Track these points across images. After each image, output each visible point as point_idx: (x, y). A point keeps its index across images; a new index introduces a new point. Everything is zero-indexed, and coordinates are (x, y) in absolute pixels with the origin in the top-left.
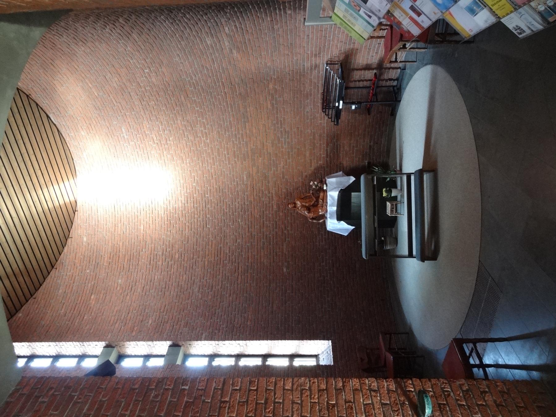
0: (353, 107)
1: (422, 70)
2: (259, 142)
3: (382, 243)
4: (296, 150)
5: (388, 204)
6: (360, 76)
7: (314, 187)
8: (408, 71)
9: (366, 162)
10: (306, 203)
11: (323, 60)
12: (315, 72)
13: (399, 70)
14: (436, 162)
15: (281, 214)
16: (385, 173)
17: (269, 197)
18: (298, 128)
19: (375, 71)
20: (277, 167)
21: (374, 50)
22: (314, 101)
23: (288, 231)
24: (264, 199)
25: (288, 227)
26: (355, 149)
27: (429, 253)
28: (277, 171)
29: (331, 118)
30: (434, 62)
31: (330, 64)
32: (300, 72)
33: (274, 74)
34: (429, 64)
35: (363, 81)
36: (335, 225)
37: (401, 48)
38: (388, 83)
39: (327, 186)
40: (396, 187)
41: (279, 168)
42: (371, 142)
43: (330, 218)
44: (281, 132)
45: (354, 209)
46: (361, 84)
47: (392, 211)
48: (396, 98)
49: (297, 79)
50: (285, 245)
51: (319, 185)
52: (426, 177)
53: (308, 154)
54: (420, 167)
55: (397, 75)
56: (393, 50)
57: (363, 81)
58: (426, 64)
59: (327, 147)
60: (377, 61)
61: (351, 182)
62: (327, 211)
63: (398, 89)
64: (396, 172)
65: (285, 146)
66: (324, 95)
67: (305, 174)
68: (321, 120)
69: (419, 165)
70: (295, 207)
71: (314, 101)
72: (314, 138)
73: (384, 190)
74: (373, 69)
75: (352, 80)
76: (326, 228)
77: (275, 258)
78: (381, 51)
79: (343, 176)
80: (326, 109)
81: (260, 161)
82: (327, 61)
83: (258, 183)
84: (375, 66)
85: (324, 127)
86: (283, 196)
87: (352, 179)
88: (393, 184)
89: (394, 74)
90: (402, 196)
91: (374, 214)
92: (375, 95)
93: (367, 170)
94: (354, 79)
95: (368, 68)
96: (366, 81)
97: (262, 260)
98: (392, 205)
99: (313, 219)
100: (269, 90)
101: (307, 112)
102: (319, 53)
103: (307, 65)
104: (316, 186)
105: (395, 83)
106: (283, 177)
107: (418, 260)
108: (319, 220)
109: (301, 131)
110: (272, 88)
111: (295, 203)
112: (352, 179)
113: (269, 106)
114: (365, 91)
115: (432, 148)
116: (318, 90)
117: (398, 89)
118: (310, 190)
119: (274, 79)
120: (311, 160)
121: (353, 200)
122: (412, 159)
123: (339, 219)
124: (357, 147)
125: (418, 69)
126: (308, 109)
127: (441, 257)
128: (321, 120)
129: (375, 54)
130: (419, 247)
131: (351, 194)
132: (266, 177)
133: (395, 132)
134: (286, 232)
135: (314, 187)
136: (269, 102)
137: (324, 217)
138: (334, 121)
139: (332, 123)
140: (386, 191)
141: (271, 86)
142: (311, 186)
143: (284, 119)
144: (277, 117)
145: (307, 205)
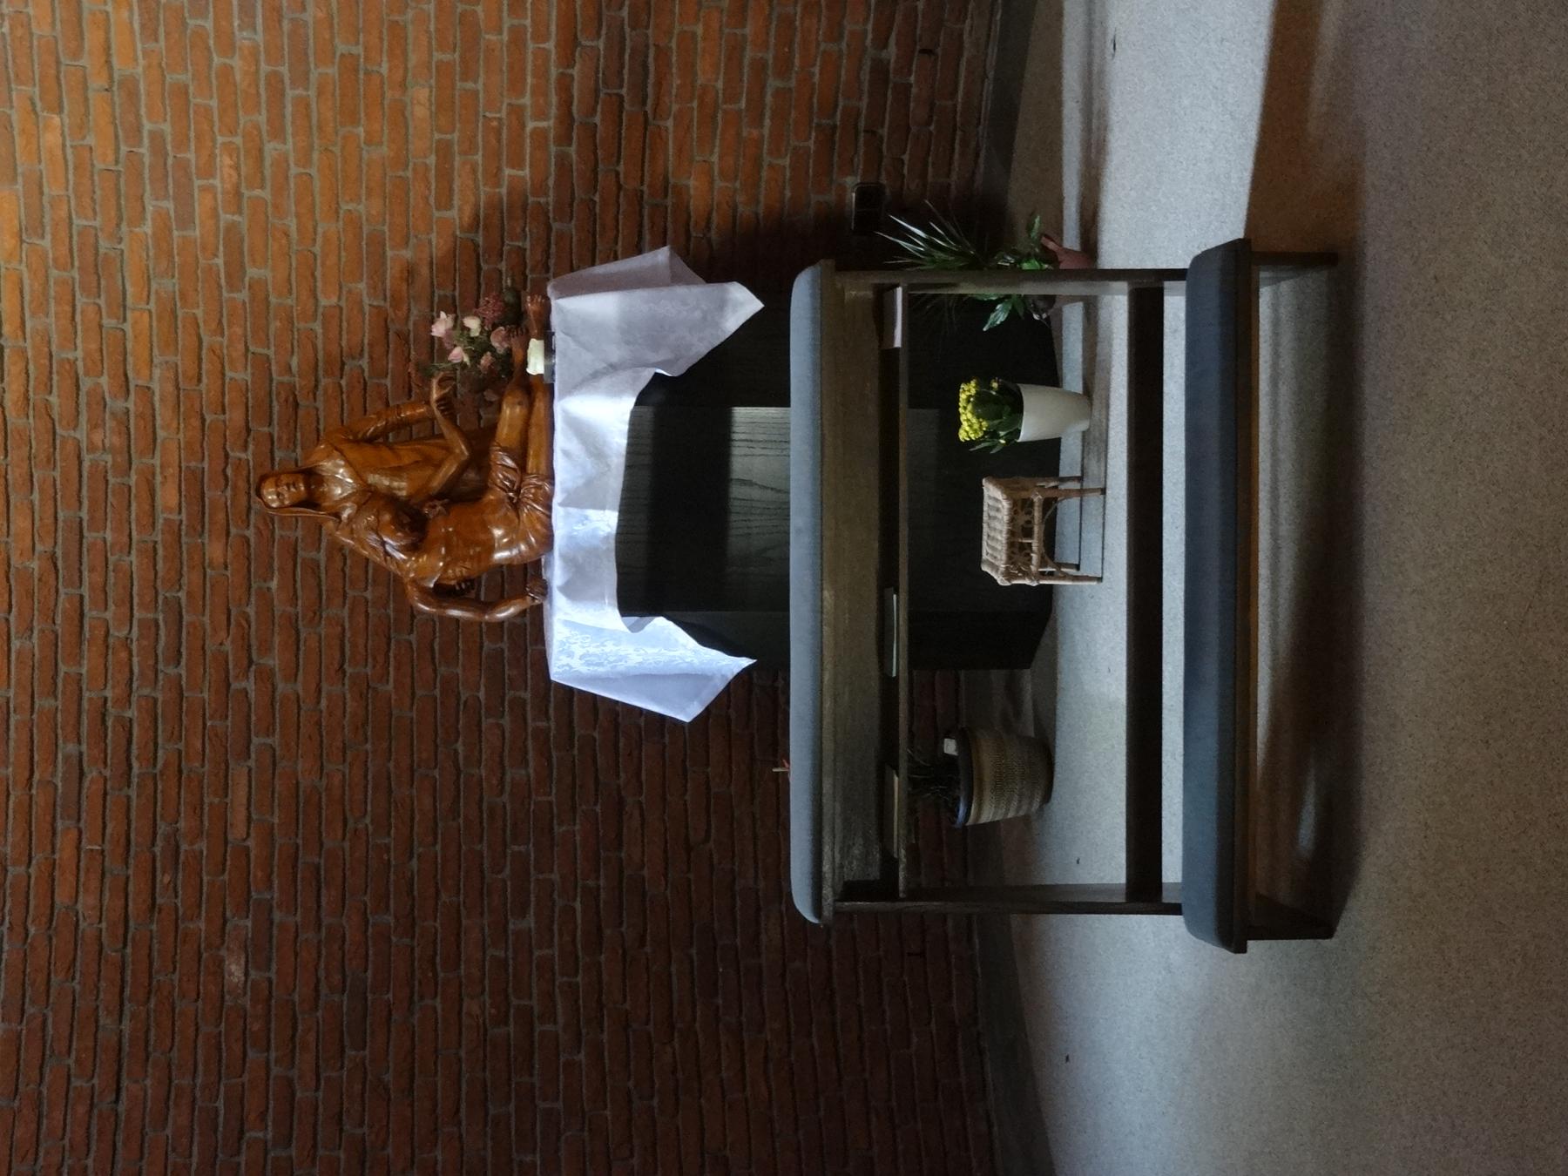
7: (458, 354)
10: (396, 472)
23: (266, 676)
25: (266, 648)
70: (311, 501)
99: (444, 593)
104: (478, 347)
111: (312, 476)
134: (251, 686)
142: (437, 349)
145: (402, 487)
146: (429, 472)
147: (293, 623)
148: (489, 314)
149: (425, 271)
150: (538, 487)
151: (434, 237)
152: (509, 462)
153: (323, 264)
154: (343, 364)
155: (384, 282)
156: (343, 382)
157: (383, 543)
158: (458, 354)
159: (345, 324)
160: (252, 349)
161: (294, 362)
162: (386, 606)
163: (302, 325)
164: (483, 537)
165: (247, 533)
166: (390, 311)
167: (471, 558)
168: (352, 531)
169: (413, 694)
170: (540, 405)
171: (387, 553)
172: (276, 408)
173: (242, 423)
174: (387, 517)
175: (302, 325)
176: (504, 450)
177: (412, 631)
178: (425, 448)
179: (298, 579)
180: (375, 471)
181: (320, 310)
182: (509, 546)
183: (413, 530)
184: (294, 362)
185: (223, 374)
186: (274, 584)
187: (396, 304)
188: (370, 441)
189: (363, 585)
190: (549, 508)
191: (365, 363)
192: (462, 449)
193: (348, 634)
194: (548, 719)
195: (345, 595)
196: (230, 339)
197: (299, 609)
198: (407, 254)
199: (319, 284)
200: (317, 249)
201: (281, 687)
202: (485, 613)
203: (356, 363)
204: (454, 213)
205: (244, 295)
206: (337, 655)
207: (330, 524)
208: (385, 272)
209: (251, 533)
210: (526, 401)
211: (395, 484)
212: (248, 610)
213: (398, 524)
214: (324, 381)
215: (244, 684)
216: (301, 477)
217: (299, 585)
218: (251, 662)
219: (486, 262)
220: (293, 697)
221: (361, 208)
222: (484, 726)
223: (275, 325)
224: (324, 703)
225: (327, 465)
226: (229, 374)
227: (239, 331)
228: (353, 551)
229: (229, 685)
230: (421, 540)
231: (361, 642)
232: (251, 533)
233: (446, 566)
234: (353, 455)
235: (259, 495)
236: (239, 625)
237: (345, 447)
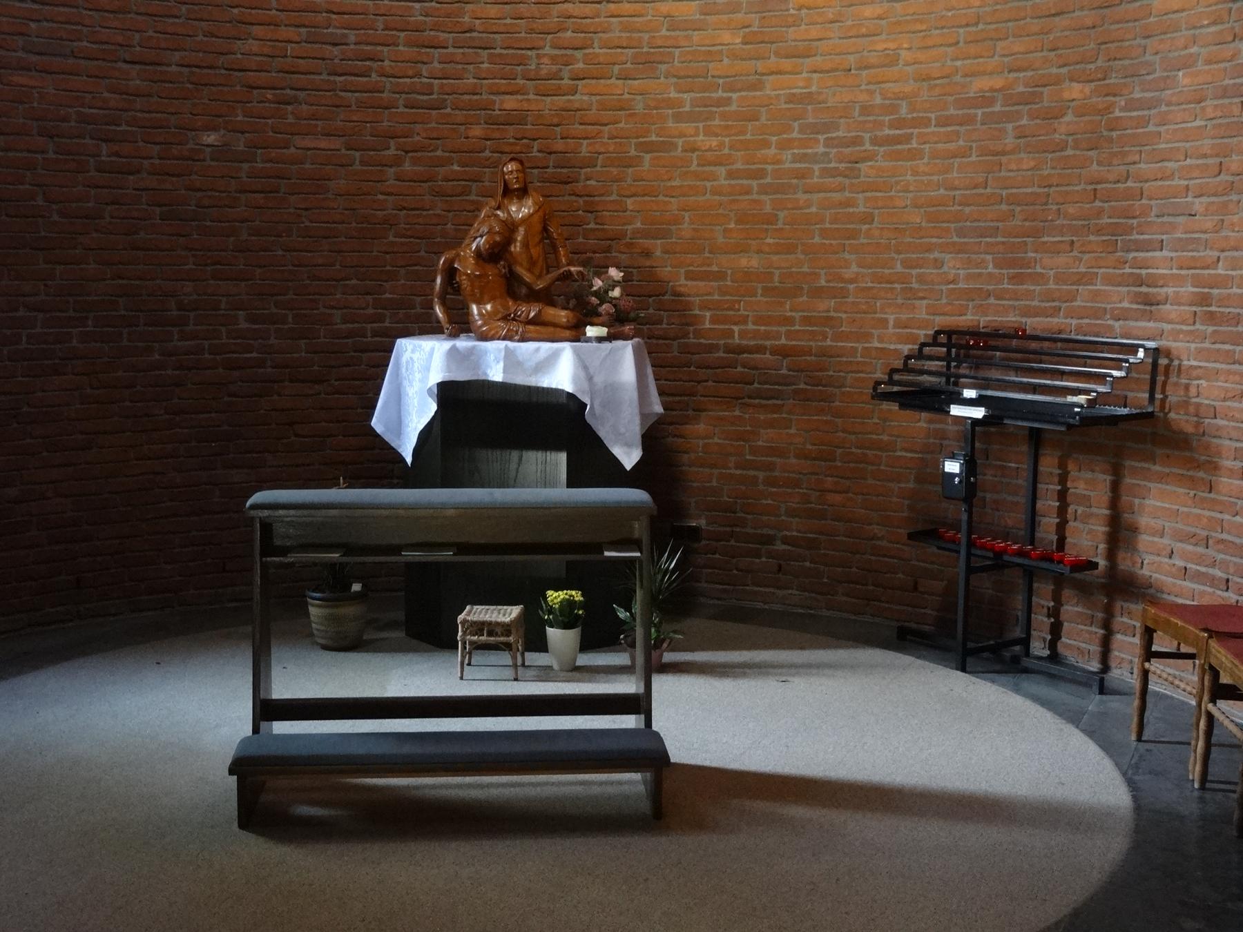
0: (952, 467)
1: (1107, 764)
2: (814, 32)
3: (335, 583)
4: (768, 208)
5: (510, 613)
6: (1085, 500)
7: (598, 283)
8: (1093, 703)
9: (702, 523)
10: (526, 245)
11: (1175, 335)
12: (1121, 297)
13: (1095, 666)
14: (699, 824)
15: (477, 131)
16: (656, 602)
17: (556, 76)
18: (868, 219)
19: (1102, 563)
20: (691, 117)
21: (1200, 560)
22: (989, 294)
23: (397, 161)
24: (548, 50)
25: (415, 162)
26: (761, 475)
27: (270, 792)
28: (678, 118)
29: (906, 369)
30: (1149, 822)
31: (1155, 365)
32: (1129, 230)
33: (1131, 105)
34: (1135, 799)
35: (1062, 511)
36: (420, 370)
37: (1215, 674)
38: (1041, 621)
39: (600, 340)
40: (586, 645)
41: (687, 127)
42: (785, 541)
43: (453, 350)
44: (856, 141)
45: (491, 459)
46: (1048, 504)
47: (479, 627)
48: (975, 652)
49: (1099, 213)
50: (336, 143)
51: (605, 307)
52: (630, 783)
53: (749, 262)
54: (677, 754)
55: (1071, 657)
56: (1213, 644)
57: (1062, 511)
58: (1131, 784)
59: (776, 351)
60: (1146, 572)
61: (617, 451)
62: (484, 338)
63: (1015, 660)
64: (654, 646)
65: (787, 155)
66: (1015, 336)
67: (657, 246)
68: (899, 324)
69: (681, 750)
70: (507, 192)
71: (989, 294)
72: (818, 293)
73: (577, 596)
74: (1111, 555)
75: (1071, 466)
76: (407, 334)
77: (269, 95)
78: (1188, 592)
79: (644, 416)
80: (949, 346)
81: (726, 37)
82: (1168, 354)
83: (625, 29)
84: (1124, 563)
85: (867, 337)
86: (559, 145)
87: (629, 457)
88: (599, 632)
89: (1080, 643)
90: (545, 674)
91: (462, 548)
92: (998, 562)
93: (668, 524)
94: (1073, 474)
95: (1120, 532)
96: (1061, 528)
97: (256, 30)
98: (506, 629)
99: (451, 273)
100: (1058, 81)
101: (938, 264)
102: (1211, 318)
103: (1161, 262)
104: (602, 295)
105: (1039, 648)
106: (648, 148)
107: (245, 741)
108: (443, 303)
109: (853, 235)
110: (1066, 95)
111: (523, 193)
112: (629, 457)
113: (981, 84)
114: (1014, 519)
115: (760, 806)
116: (1037, 313)
117: (1015, 660)
118: (584, 264)
119: (1109, 109)
120: (720, 276)
121: (533, 460)
122: (713, 717)
123: (448, 393)
124: (771, 482)
125: (1108, 746)
126: (952, 265)
127: (254, 847)
128: (899, 324)
129: (1181, 563)
130: (305, 752)
131: (557, 448)
132: (648, 64)
133: (837, 647)
134: (392, 152)
135: (598, 283)
136: (998, 82)
137: (460, 325)
138: (891, 382)
139: (880, 375)
140: (569, 604)
141: (1075, 91)
142: (601, 271)
143: (914, 155)
144: (926, 122)
145: (516, 248)
146: (525, 264)
149: (648, 263)
150: (517, 332)
151: (669, 269)
152: (532, 314)
157: (482, 236)
161: (593, 182)
163: (615, 187)
164: (486, 297)
170: (567, 333)
172: (565, 171)
174: (498, 239)
175: (615, 187)
184: (593, 182)
186: (456, 167)
188: (545, 229)
190: (504, 339)
191: (592, 226)
192: (540, 285)
198: (658, 253)
199: (639, 199)
200: (661, 198)
204: (683, 281)
205: (633, 153)
209: (487, 153)
214: (581, 201)
215: (393, 148)
218: (407, 152)
221: (686, 225)
223: (615, 171)
224: (381, 197)
226: (585, 142)
228: (477, 216)
230: (483, 259)
231: (421, 220)
232: (487, 153)
234: (536, 218)
235: (512, 160)
237: (541, 213)
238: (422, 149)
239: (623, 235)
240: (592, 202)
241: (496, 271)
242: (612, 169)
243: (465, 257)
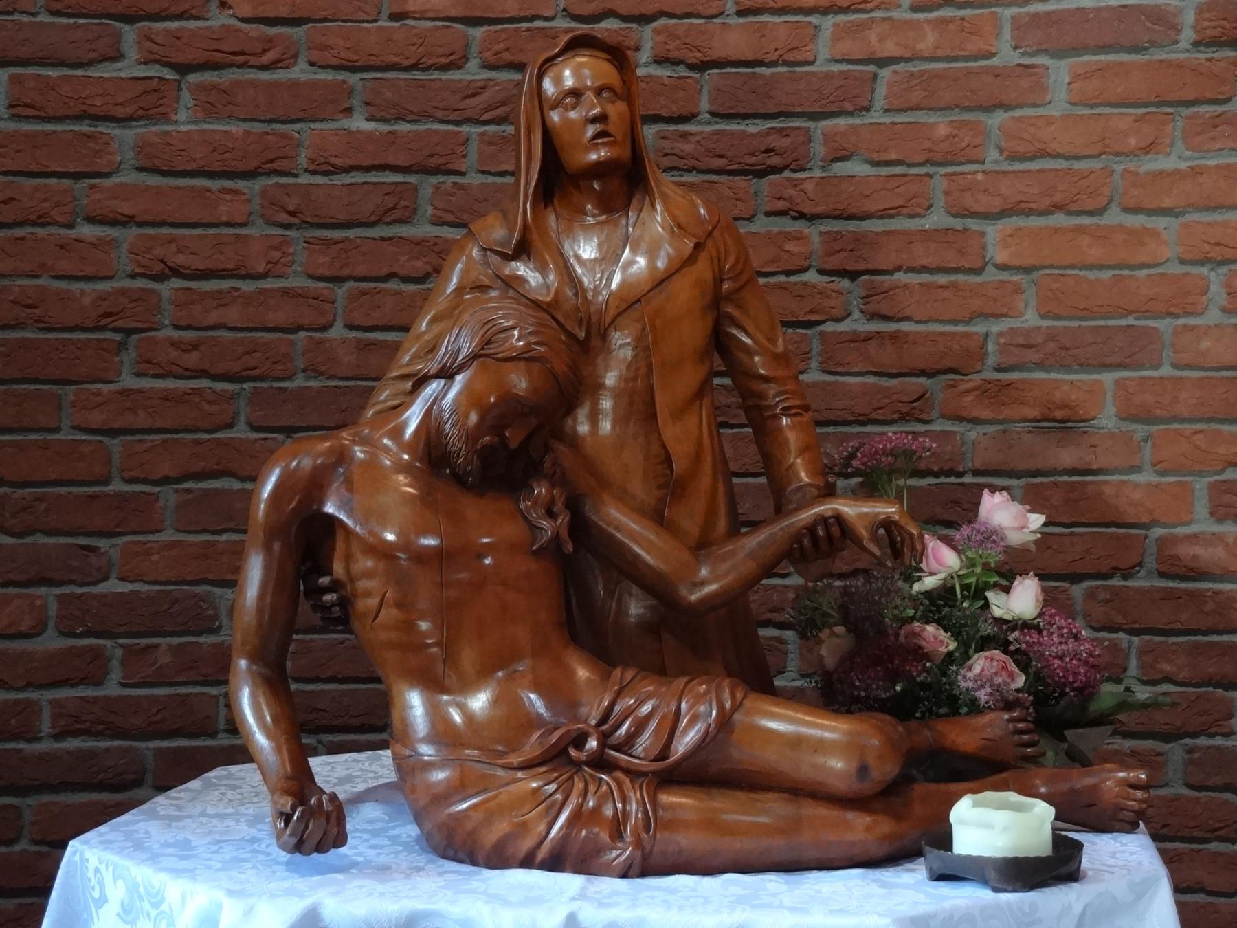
7: (942, 562)
10: (641, 408)
23: (149, 104)
25: (214, 104)
67: (1102, 394)
70: (558, 182)
99: (308, 541)
104: (953, 605)
111: (623, 185)
134: (129, 68)
142: (953, 513)
145: (599, 423)
146: (639, 488)
147: (271, 165)
148: (1052, 645)
149: (1067, 457)
150: (617, 828)
151: (1146, 477)
152: (686, 740)
153: (1081, 230)
154: (853, 275)
155: (1040, 366)
156: (811, 276)
157: (447, 374)
158: (942, 562)
159: (942, 279)
160: (886, 73)
161: (855, 167)
162: (312, 370)
163: (939, 185)
164: (468, 657)
165: (473, 64)
166: (976, 379)
167: (409, 626)
168: (483, 288)
169: (113, 433)
170: (860, 828)
171: (421, 381)
172: (754, 127)
173: (718, 52)
174: (520, 382)
175: (939, 185)
176: (725, 722)
177: (255, 428)
178: (705, 481)
179: (373, 177)
180: (643, 347)
181: (973, 224)
182: (443, 734)
183: (487, 456)
184: (855, 167)
185: (825, 11)
186: (359, 123)
187: (995, 392)
188: (719, 343)
189: (359, 320)
190: (555, 863)
191: (856, 324)
192: (707, 582)
193: (247, 287)
194: (57, 737)
195: (337, 280)
196: (910, 24)
197: (304, 179)
198: (1107, 419)
199: (1034, 222)
200: (1114, 217)
201: (125, 136)
202: (253, 658)
203: (855, 304)
204: (1202, 524)
205: (1007, 55)
206: (198, 264)
207: (497, 231)
208: (1066, 368)
209: (473, 72)
210: (867, 787)
211: (606, 404)
212: (302, 64)
213: (500, 415)
214: (814, 233)
215: (132, 53)
216: (624, 153)
217: (358, 178)
218: (183, 69)
219: (1090, 595)
220: (101, 164)
221: (1213, 316)
222: (43, 590)
223: (940, 124)
224: (87, 231)
225: (656, 221)
226: (828, 23)
227: (927, 43)
228: (426, 297)
229: (130, 19)
230: (459, 480)
231: (232, 314)
232: (473, 72)
233: (384, 552)
234: (684, 292)
235: (577, 44)
236: (270, 43)
237: (703, 269)
238: (240, 58)
239: (974, 355)
240: (858, 239)
241: (512, 530)
242: (932, 118)
243: (371, 464)
